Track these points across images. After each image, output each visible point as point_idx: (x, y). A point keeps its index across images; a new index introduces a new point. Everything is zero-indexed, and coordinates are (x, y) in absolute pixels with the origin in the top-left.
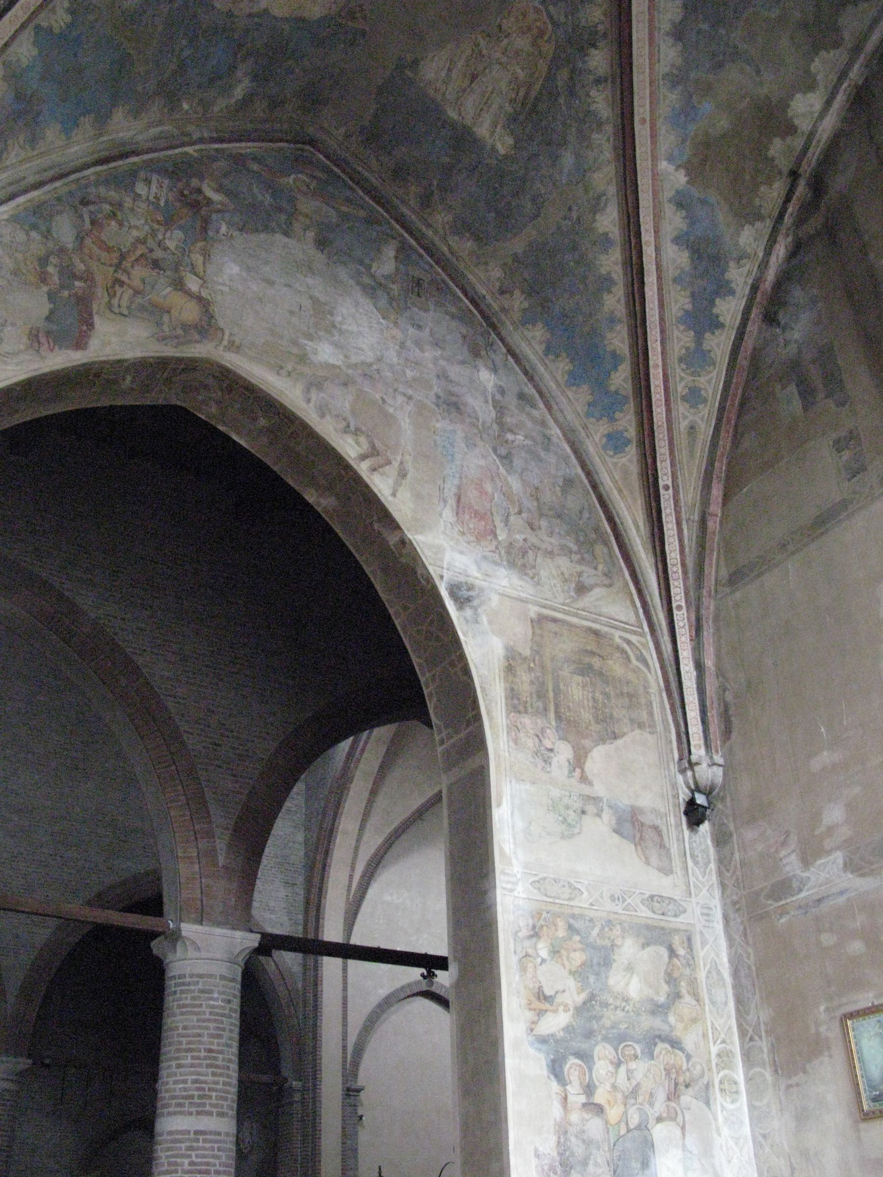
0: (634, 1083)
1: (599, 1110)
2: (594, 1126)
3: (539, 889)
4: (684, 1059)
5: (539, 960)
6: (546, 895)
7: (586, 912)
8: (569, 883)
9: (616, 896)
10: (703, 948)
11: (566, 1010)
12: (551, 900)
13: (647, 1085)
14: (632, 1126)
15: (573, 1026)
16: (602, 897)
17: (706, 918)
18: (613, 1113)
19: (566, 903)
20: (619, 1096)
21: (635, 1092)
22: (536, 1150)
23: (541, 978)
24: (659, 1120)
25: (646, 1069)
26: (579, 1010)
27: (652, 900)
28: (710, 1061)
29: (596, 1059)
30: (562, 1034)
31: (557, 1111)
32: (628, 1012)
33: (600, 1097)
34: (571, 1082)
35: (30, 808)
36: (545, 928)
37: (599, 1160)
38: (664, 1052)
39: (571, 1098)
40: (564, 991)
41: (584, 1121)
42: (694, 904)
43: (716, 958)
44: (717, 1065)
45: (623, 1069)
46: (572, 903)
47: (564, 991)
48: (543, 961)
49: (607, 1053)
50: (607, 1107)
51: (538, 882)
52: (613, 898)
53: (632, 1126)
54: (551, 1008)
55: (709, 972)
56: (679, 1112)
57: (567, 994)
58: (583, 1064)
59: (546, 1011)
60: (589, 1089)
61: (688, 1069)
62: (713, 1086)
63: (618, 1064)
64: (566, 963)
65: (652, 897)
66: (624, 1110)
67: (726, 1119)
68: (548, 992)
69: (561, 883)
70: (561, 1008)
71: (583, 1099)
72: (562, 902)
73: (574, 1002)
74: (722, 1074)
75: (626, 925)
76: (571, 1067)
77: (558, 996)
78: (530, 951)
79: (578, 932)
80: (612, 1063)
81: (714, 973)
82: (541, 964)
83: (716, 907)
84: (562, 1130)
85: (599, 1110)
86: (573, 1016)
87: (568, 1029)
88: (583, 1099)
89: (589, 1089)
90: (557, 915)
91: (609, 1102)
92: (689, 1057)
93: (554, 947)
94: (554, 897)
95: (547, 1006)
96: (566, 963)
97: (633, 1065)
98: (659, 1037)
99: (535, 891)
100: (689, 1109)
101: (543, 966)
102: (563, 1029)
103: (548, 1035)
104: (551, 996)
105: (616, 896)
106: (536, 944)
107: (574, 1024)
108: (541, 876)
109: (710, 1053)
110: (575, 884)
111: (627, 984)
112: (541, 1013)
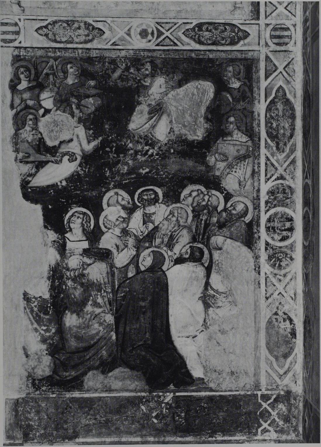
0: (151, 226)
1: (105, 256)
2: (97, 271)
3: (46, 35)
4: (222, 200)
5: (42, 111)
6: (55, 41)
7: (107, 54)
8: (85, 23)
9: (150, 31)
10: (267, 78)
11: (72, 157)
12: (62, 45)
13: (166, 228)
14: (143, 268)
15: (79, 175)
16: (129, 35)
17: (276, 41)
18: (121, 259)
19: (80, 46)
20: (131, 241)
21: (150, 237)
22: (25, 294)
23: (41, 129)
24: (180, 261)
25: (168, 213)
26: (87, 159)
27: (200, 29)
28: (258, 198)
29: (105, 206)
30: (64, 183)
31: (52, 256)
32: (152, 155)
33: (108, 241)
34: (71, 230)
35: (230, 167)
36: (51, 77)
37: (100, 300)
38: (194, 194)
39: (69, 245)
40: (71, 140)
41: (85, 266)
42: (263, 27)
43: (284, 86)
44: (267, 202)
45: (138, 215)
46: (89, 46)
47: (71, 140)
48: (47, 111)
49: (120, 198)
50: (114, 251)
51: (46, 27)
52: (144, 34)
53: (143, 268)
54: (53, 159)
55: (273, 102)
56: (206, 252)
57: (75, 143)
58: (84, 210)
59: (47, 162)
60: (94, 235)
61: (225, 210)
62: (258, 225)
63: (131, 210)
64: (76, 112)
65: (200, 26)
66: (135, 253)
67: (270, 258)
68: (50, 143)
69: (76, 25)
70: (66, 158)
71: (85, 245)
72: (75, 46)
73: (82, 150)
74: (272, 211)
75: (158, 62)
76: (72, 215)
77: (63, 146)
78: (30, 103)
79: (92, 76)
80: (124, 208)
81: (280, 106)
82: (43, 116)
83: (294, 26)
84: (56, 274)
85: (105, 256)
86: (80, 165)
87: (73, 179)
88: (85, 245)
89: (94, 235)
90: (69, 61)
91: (117, 247)
92: (228, 197)
93: (61, 96)
94: (67, 42)
95: (49, 157)
96: (76, 112)
97: (151, 209)
98: (184, 178)
99: (41, 38)
100: (220, 249)
101: (47, 117)
102: (66, 179)
103: (48, 186)
104: (54, 147)
105: (150, 31)
106: (38, 96)
107: (81, 173)
108: (50, 20)
109: (258, 191)
110: (93, 23)
111: (153, 127)
112: (40, 165)
